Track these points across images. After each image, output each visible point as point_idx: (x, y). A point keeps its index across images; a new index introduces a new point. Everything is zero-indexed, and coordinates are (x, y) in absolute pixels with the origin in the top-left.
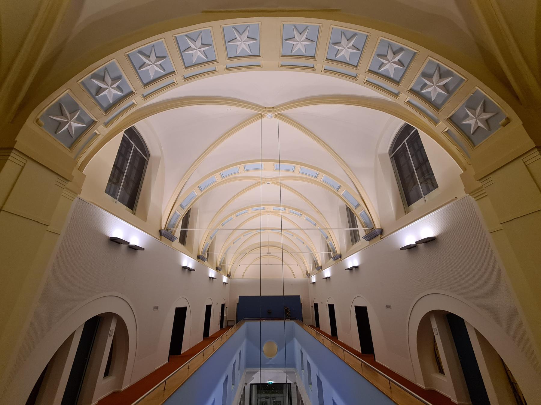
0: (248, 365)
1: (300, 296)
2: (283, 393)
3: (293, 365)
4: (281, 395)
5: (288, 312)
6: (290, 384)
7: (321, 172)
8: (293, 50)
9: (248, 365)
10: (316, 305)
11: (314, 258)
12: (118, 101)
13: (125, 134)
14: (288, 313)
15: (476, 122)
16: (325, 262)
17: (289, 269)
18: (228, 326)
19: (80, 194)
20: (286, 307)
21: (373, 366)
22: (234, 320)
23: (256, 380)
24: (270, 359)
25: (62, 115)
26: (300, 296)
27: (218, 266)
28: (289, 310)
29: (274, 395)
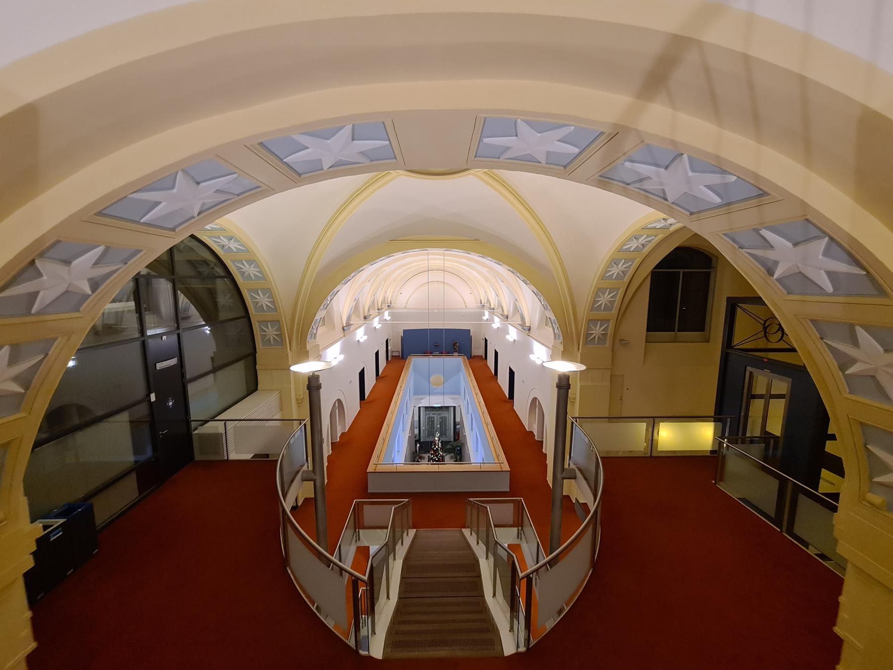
0: (416, 393)
2: (448, 411)
3: (459, 393)
4: (447, 412)
9: (416, 393)
10: (486, 340)
12: (280, 329)
13: (842, 577)
15: (139, 250)
16: (539, 325)
18: (392, 356)
19: (194, 458)
21: (803, 549)
23: (425, 403)
24: (437, 388)
25: (667, 220)
29: (439, 412)
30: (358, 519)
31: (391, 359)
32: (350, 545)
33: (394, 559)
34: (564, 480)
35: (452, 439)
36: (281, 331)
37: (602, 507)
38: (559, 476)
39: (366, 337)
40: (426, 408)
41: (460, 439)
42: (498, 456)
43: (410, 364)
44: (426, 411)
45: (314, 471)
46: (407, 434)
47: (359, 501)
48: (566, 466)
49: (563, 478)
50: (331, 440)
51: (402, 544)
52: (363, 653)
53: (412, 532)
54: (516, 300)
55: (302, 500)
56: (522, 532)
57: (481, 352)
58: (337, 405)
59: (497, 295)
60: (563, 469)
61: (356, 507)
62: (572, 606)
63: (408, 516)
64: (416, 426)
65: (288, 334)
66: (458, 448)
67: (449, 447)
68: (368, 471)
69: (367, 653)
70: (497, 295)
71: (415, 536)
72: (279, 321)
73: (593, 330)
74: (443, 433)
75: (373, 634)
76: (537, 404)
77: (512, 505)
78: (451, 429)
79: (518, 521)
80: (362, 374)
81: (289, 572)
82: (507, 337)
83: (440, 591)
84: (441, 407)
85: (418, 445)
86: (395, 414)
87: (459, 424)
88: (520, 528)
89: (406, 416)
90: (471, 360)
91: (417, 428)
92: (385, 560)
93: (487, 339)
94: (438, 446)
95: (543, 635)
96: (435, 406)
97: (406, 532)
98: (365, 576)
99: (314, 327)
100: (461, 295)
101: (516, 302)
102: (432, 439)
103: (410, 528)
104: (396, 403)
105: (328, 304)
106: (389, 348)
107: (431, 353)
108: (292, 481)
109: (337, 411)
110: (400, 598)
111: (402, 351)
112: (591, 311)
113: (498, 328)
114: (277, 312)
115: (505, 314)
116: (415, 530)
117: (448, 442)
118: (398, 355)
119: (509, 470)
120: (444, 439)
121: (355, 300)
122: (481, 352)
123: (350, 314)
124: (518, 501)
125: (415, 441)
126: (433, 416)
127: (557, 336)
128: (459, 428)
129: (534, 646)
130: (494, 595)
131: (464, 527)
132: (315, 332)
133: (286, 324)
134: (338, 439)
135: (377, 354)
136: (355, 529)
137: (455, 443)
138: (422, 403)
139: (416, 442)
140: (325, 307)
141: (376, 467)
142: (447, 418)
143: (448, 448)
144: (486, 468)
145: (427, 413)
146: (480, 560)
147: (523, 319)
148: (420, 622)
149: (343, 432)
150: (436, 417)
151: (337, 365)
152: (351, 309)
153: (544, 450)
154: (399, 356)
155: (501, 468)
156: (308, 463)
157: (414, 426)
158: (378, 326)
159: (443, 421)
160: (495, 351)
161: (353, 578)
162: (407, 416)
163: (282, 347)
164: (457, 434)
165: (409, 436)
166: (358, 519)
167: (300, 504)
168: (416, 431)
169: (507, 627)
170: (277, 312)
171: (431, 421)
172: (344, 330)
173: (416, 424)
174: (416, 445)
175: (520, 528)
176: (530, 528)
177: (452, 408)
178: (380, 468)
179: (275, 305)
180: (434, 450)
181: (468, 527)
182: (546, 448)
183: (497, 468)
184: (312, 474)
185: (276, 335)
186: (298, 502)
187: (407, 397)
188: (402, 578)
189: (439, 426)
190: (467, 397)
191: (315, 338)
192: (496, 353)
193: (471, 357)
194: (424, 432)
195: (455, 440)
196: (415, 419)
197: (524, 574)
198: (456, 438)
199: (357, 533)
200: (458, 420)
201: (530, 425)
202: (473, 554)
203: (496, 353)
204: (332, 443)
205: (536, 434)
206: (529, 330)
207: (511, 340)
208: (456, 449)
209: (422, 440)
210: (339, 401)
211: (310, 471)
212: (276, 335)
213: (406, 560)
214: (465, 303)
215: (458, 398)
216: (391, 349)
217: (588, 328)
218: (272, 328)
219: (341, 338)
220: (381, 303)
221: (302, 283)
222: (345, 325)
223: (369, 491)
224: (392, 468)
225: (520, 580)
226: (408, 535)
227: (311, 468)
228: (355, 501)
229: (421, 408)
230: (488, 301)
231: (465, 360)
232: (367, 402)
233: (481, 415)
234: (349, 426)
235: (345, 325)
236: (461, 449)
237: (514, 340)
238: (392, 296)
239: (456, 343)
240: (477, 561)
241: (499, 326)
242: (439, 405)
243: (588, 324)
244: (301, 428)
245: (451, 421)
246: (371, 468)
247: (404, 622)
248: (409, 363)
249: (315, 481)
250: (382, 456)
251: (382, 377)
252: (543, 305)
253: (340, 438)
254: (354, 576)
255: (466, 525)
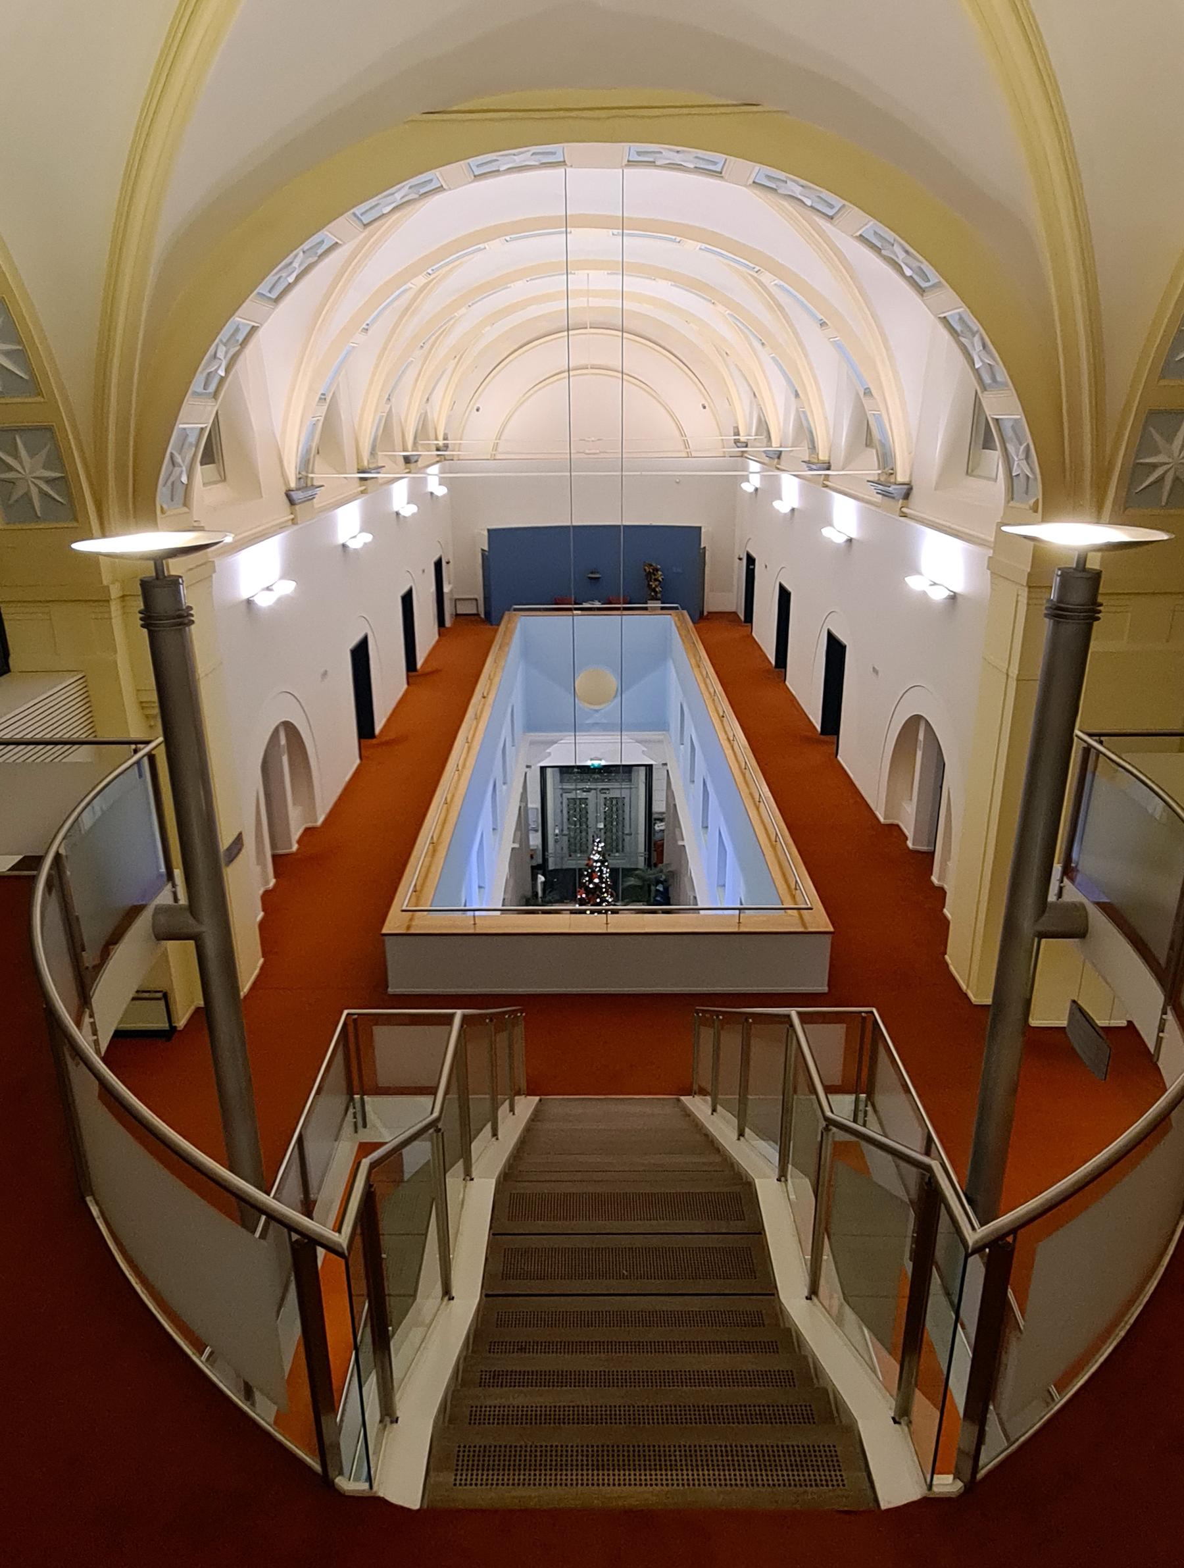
1: (700, 528)
5: (656, 580)
6: (651, 766)
7: (218, 333)
8: (357, 1325)
10: (751, 560)
11: (802, 415)
12: (57, 459)
14: (657, 583)
16: (941, 475)
17: (673, 424)
18: (457, 615)
20: (651, 565)
22: (476, 596)
23: (562, 753)
24: (597, 711)
26: (700, 528)
27: (366, 463)
28: (660, 573)
29: (601, 786)
30: (360, 1070)
31: (454, 624)
32: (336, 1138)
33: (468, 1175)
34: (1044, 941)
35: (641, 863)
36: (62, 467)
37: (362, 1234)
38: (1027, 925)
39: (367, 538)
40: (565, 771)
41: (665, 861)
42: (792, 892)
43: (512, 633)
44: (562, 781)
45: (192, 908)
46: (507, 842)
47: (359, 1014)
48: (1052, 898)
49: (1042, 935)
50: (273, 845)
51: (495, 1134)
52: (349, 1484)
53: (526, 1105)
54: (868, 392)
55: (187, 1016)
56: (869, 1108)
57: (733, 602)
58: (283, 741)
59: (797, 395)
60: (1042, 905)
61: (351, 1029)
62: (1124, 1339)
63: (511, 1056)
64: (533, 826)
65: (88, 477)
66: (660, 888)
67: (632, 881)
68: (384, 931)
69: (366, 1486)
70: (797, 395)
71: (537, 1116)
72: (49, 429)
73: (1157, 452)
74: (614, 845)
75: (387, 1419)
76: (921, 736)
77: (839, 1030)
78: (637, 834)
79: (859, 1077)
80: (360, 655)
81: (95, 1211)
82: (827, 532)
83: (624, 1277)
84: (607, 769)
85: (541, 878)
86: (467, 773)
87: (661, 820)
88: (863, 1096)
89: (502, 789)
90: (700, 625)
91: (537, 831)
92: (436, 1175)
93: (754, 555)
94: (601, 878)
95: (1023, 1439)
96: (589, 763)
97: (507, 1103)
98: (339, 1231)
99: (178, 459)
100: (672, 415)
101: (866, 402)
102: (583, 863)
103: (519, 1093)
104: (469, 742)
105: (222, 380)
106: (446, 589)
107: (576, 604)
108: (115, 938)
109: (285, 759)
110: (488, 1295)
111: (487, 599)
112: (1163, 376)
113: (793, 510)
114: (40, 394)
115: (821, 458)
116: (537, 1098)
117: (628, 872)
118: (474, 611)
119: (832, 929)
120: (617, 861)
121: (323, 399)
122: (733, 602)
123: (308, 451)
124: (864, 1018)
125: (533, 868)
126: (584, 795)
127: (1019, 485)
128: (662, 831)
129: (990, 1472)
130: (813, 1292)
131: (689, 1092)
132: (184, 479)
133: (74, 427)
134: (295, 847)
135: (407, 599)
136: (350, 1093)
137: (650, 872)
138: (550, 754)
139: (535, 870)
140: (212, 388)
141: (411, 919)
142: (627, 801)
143: (630, 886)
144: (754, 922)
145: (567, 786)
146: (758, 1183)
147: (886, 460)
148: (561, 1379)
149: (310, 825)
150: (595, 798)
151: (271, 608)
152: (312, 433)
153: (934, 879)
154: (478, 615)
155: (804, 924)
156: (174, 886)
157: (527, 824)
158: (409, 510)
159: (615, 811)
160: (782, 588)
161: (295, 1237)
162: (504, 787)
163: (76, 525)
164: (655, 848)
165: (513, 849)
166: (360, 1070)
167: (181, 1023)
168: (535, 840)
169: (886, 1407)
170: (40, 394)
171: (577, 810)
172: (292, 502)
173: (534, 819)
174: (534, 879)
175: (863, 1096)
176: (903, 1096)
177: (642, 771)
178: (423, 923)
179: (26, 365)
180: (588, 891)
181: (702, 1092)
182: (943, 870)
183: (788, 921)
184: (188, 914)
185: (48, 481)
186: (174, 1018)
187: (505, 732)
188: (495, 1233)
189: (601, 826)
190: (691, 730)
191: (185, 504)
192: (784, 596)
193: (702, 618)
194: (556, 841)
195: (649, 863)
196: (530, 805)
197: (983, 1231)
198: (654, 860)
199: (358, 1105)
200: (659, 806)
201: (892, 803)
202: (729, 1164)
203: (784, 596)
204: (275, 857)
205: (909, 831)
206: (907, 496)
207: (840, 539)
208: (653, 888)
209: (551, 866)
210: (289, 727)
211: (181, 908)
212: (48, 481)
213: (506, 1179)
214: (682, 434)
215: (660, 742)
216: (451, 591)
217: (1144, 445)
218: (31, 456)
219: (280, 528)
220: (415, 438)
221: (117, 276)
222: (293, 485)
223: (390, 990)
224: (461, 923)
225: (967, 1256)
226: (512, 1110)
227: (183, 900)
228: (346, 1012)
229: (549, 771)
230: (763, 428)
231: (683, 621)
232: (378, 745)
233: (739, 779)
234: (328, 810)
235: (293, 485)
236: (666, 889)
237: (850, 540)
238: (449, 417)
239: (657, 570)
240: (750, 1186)
241: (796, 504)
242: (603, 763)
243: (1145, 428)
244: (138, 762)
245: (637, 810)
246: (394, 923)
247: (497, 1379)
248: (509, 632)
249: (196, 938)
250: (429, 892)
251: (425, 675)
252: (977, 372)
253: (299, 842)
254: (297, 1232)
255: (695, 1087)
